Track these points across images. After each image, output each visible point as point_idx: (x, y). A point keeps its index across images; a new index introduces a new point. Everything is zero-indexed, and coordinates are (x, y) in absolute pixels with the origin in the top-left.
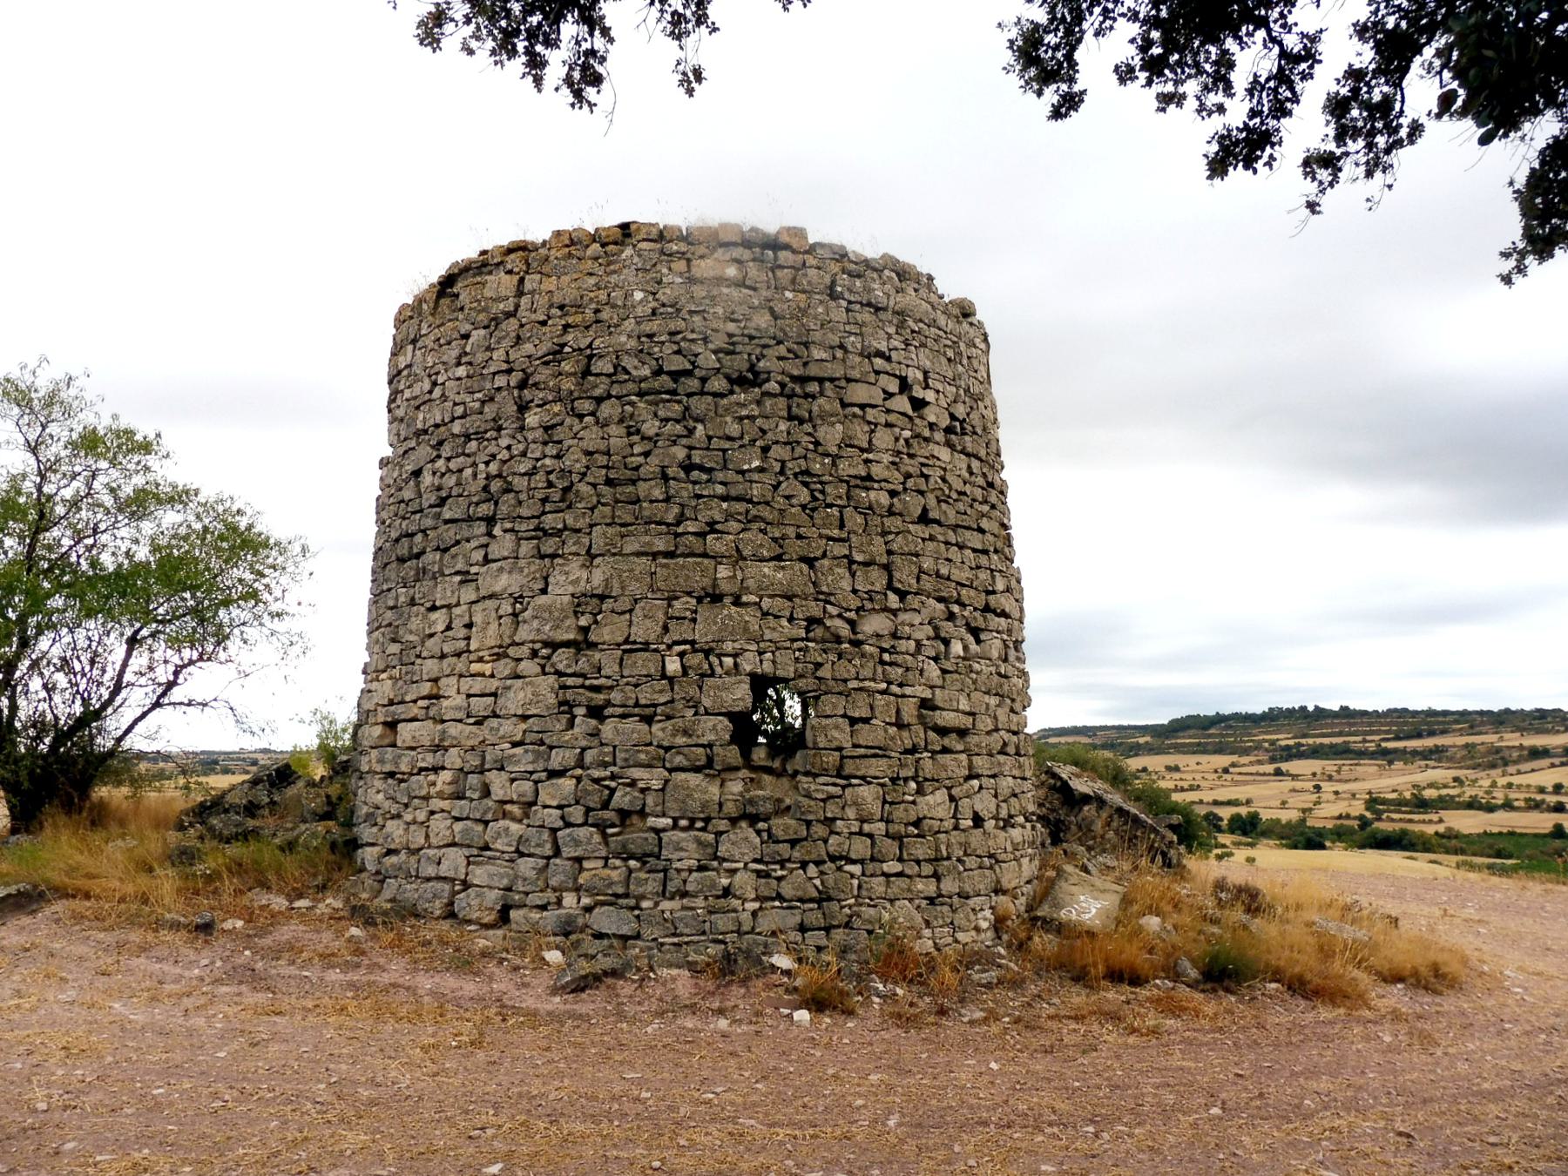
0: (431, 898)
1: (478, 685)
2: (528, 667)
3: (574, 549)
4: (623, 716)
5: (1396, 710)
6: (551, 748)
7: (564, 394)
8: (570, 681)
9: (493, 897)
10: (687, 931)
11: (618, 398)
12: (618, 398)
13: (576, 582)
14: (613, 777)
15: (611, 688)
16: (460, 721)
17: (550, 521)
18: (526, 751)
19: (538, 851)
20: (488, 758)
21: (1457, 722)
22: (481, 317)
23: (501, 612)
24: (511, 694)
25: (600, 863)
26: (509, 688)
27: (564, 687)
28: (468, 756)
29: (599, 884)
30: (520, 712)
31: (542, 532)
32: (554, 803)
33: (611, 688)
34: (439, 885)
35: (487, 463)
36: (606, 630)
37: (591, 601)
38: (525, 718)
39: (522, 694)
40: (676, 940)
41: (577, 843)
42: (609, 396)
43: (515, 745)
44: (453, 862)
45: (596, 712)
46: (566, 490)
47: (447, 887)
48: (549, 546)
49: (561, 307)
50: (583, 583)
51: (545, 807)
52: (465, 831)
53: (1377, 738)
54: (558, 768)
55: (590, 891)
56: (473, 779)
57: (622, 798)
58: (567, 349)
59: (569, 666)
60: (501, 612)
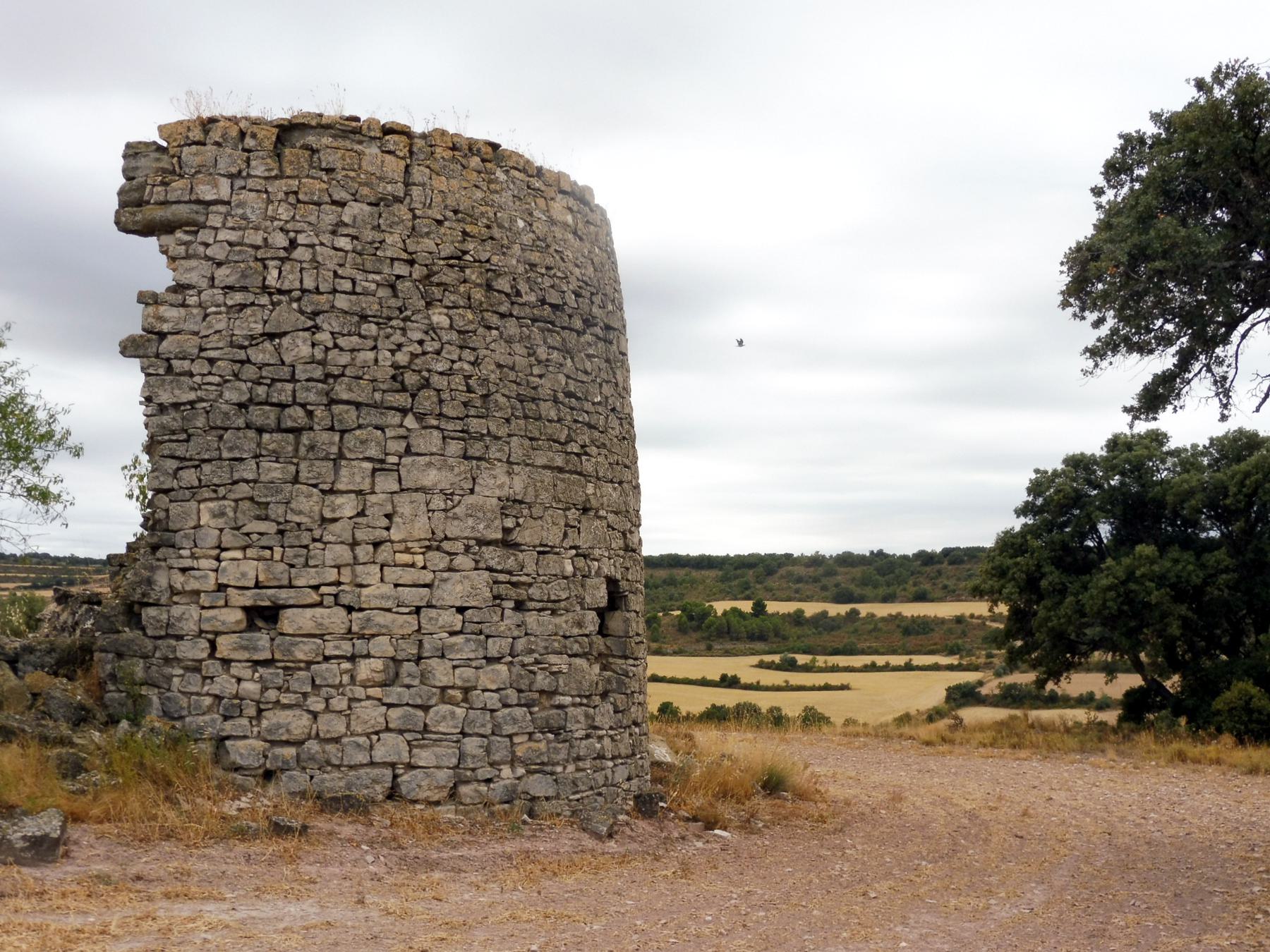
0: (373, 784)
1: (409, 576)
2: (463, 561)
3: (498, 455)
4: (540, 610)
5: (35, 555)
6: (488, 637)
7: (475, 304)
8: (502, 577)
9: (443, 776)
10: (583, 788)
11: (518, 318)
12: (518, 318)
13: (501, 486)
14: (537, 662)
15: (530, 585)
16: (389, 610)
17: (475, 425)
18: (468, 640)
19: (482, 731)
20: (426, 646)
21: (98, 572)
22: (365, 191)
23: (432, 506)
24: (448, 586)
25: (526, 737)
26: (445, 580)
27: (495, 582)
29: (533, 755)
30: (458, 604)
31: (466, 435)
32: (494, 687)
33: (530, 585)
34: (376, 772)
35: (393, 352)
36: (527, 533)
37: (510, 504)
38: (461, 610)
39: (459, 588)
40: (578, 796)
41: (515, 721)
42: (511, 315)
43: (452, 634)
44: (391, 748)
45: (519, 606)
46: (485, 397)
47: (388, 772)
48: (476, 449)
49: (456, 212)
50: (506, 488)
51: (484, 691)
52: (405, 717)
53: (11, 585)
54: (496, 655)
55: (524, 763)
57: (542, 681)
58: (468, 257)
59: (499, 563)
60: (432, 506)
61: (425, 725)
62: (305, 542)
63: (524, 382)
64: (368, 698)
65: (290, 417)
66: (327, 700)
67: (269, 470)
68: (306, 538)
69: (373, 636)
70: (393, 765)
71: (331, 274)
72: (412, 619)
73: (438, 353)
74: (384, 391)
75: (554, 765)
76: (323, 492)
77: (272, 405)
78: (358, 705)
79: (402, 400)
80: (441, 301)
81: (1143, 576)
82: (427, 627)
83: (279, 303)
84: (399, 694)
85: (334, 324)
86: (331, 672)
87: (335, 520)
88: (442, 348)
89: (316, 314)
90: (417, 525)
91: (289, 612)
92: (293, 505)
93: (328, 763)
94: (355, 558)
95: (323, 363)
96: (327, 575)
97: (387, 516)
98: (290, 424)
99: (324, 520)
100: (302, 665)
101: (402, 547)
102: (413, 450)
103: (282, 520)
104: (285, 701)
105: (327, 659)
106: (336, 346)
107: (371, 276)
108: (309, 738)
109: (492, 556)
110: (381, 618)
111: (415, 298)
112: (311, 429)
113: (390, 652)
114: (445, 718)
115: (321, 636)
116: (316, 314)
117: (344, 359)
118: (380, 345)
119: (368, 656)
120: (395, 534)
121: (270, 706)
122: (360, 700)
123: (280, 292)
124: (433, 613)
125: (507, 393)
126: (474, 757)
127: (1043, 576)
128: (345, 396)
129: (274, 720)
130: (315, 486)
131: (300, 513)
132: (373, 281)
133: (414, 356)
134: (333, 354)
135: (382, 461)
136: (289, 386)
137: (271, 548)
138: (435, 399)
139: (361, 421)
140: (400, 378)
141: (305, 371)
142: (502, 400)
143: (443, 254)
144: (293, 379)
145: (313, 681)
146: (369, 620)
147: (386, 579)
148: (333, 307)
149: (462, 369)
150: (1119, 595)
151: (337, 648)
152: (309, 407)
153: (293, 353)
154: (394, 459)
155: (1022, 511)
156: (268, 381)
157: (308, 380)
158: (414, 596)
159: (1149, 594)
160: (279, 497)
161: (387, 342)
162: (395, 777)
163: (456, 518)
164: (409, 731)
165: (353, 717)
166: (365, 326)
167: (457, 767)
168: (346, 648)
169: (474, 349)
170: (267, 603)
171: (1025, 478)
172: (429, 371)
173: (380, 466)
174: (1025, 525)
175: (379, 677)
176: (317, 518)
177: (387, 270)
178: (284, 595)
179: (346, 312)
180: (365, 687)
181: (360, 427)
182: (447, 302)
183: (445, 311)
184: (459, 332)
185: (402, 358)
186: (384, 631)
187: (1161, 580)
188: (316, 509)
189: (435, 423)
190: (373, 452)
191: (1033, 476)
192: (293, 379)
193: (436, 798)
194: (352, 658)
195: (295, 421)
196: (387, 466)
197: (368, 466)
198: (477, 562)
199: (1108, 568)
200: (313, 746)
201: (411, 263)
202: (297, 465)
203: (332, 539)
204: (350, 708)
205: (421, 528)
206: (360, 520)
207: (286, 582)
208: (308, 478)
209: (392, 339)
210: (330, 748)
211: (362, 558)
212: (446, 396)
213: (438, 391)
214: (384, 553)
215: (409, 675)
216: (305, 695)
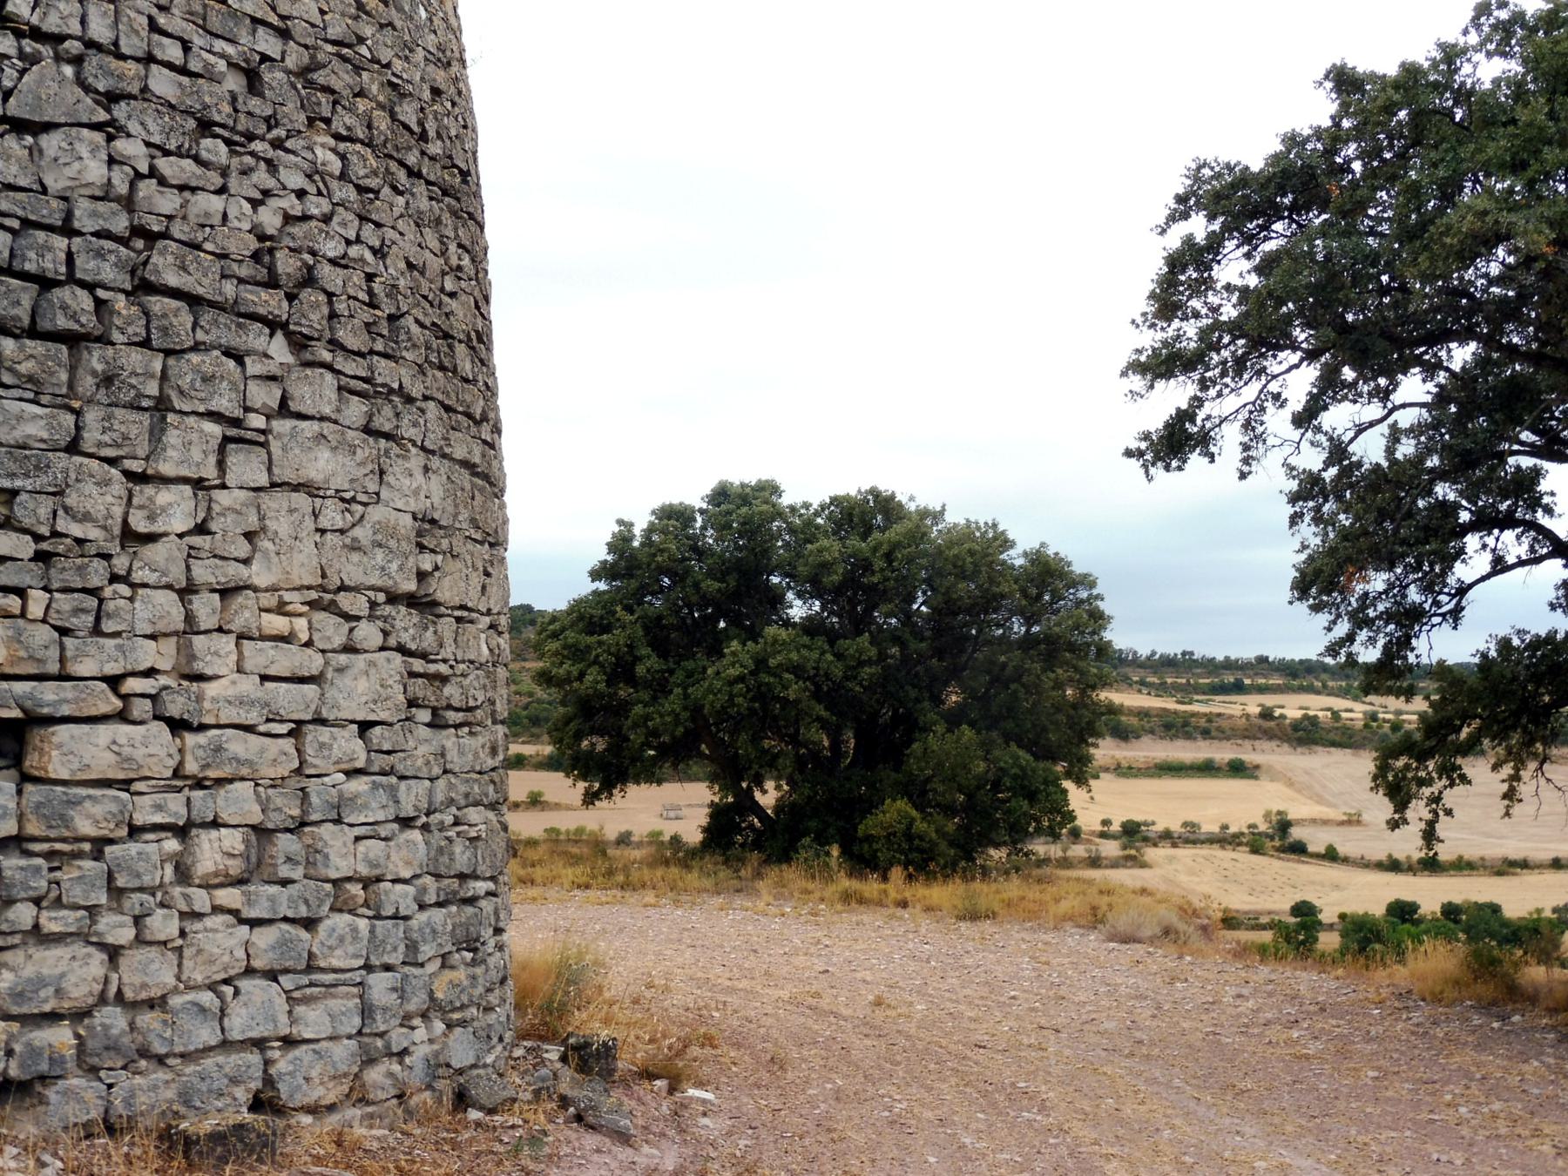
8: (418, 665)
11: (428, 183)
16: (249, 729)
20: (314, 799)
23: (324, 523)
24: (345, 681)
26: (340, 670)
27: (412, 675)
28: (277, 798)
30: (360, 717)
34: (233, 1060)
35: (255, 204)
38: (365, 727)
39: (362, 685)
43: (351, 773)
46: (392, 318)
47: (254, 1058)
52: (284, 943)
56: (286, 844)
61: (311, 955)
62: (95, 582)
63: (436, 303)
64: (217, 909)
65: (64, 307)
66: (138, 920)
67: (20, 418)
68: (97, 574)
69: (220, 782)
70: (259, 1044)
71: (145, 21)
72: (288, 745)
73: (327, 219)
74: (241, 281)
75: (463, 1007)
76: (129, 475)
77: (24, 276)
78: (198, 926)
79: (271, 302)
80: (328, 121)
81: (780, 665)
82: (316, 762)
83: (34, 59)
84: (272, 899)
85: (152, 127)
86: (148, 858)
87: (151, 538)
88: (332, 213)
89: (111, 98)
90: (299, 558)
91: (63, 732)
92: (72, 500)
93: (144, 1053)
94: (189, 618)
95: (128, 203)
96: (140, 654)
97: (249, 536)
98: (62, 322)
99: (130, 537)
100: (87, 847)
101: (269, 600)
102: (293, 406)
103: (44, 530)
104: (54, 927)
105: (135, 831)
106: (153, 172)
107: (220, 45)
108: (102, 1000)
109: (405, 623)
110: (239, 745)
111: (291, 105)
112: (104, 340)
113: (256, 817)
114: (341, 939)
115: (125, 785)
116: (111, 98)
117: (168, 202)
118: (234, 183)
119: (216, 824)
120: (259, 574)
121: (17, 939)
122: (198, 916)
123: (37, 34)
124: (324, 733)
125: (421, 317)
126: (385, 1009)
127: (638, 659)
128: (172, 279)
129: (29, 971)
130: (112, 462)
131: (86, 518)
132: (222, 56)
133: (288, 219)
134: (147, 188)
135: (236, 423)
136: (60, 243)
137: (21, 592)
138: (326, 310)
139: (200, 335)
140: (267, 259)
141: (94, 214)
142: (415, 329)
143: (332, 33)
144: (67, 230)
145: (110, 877)
146: (219, 749)
147: (248, 666)
148: (145, 89)
149: (362, 260)
150: (749, 690)
151: (159, 808)
152: (101, 293)
153: (70, 172)
154: (257, 421)
155: (595, 575)
156: (16, 224)
157: (97, 234)
158: (294, 701)
159: (785, 688)
160: (41, 481)
161: (246, 181)
162: (267, 1063)
163: (355, 547)
164: (286, 971)
165: (187, 952)
166: (207, 142)
167: (360, 1033)
168: (175, 808)
169: (378, 225)
170: (16, 713)
171: (607, 531)
172: (313, 253)
173: (235, 434)
174: (595, 593)
175: (235, 867)
176: (117, 531)
177: (245, 39)
178: (49, 695)
179: (172, 106)
180: (207, 887)
181: (196, 347)
182: (338, 126)
183: (332, 142)
184: (361, 190)
185: (269, 219)
186: (245, 771)
187: (797, 670)
188: (118, 511)
189: (326, 356)
190: (225, 403)
191: (616, 529)
192: (67, 230)
193: (330, 1098)
194: (181, 832)
195: (74, 317)
196: (249, 435)
197: (214, 429)
198: (386, 634)
199: (734, 654)
200: (113, 1019)
201: (284, 34)
202: (78, 413)
203: (152, 578)
204: (183, 934)
205: (302, 565)
206: (197, 540)
207: (53, 668)
208: (100, 444)
209: (255, 177)
210: (147, 1019)
211: (206, 620)
212: (341, 307)
213: (330, 295)
214: (244, 613)
215: (289, 859)
216: (92, 911)
